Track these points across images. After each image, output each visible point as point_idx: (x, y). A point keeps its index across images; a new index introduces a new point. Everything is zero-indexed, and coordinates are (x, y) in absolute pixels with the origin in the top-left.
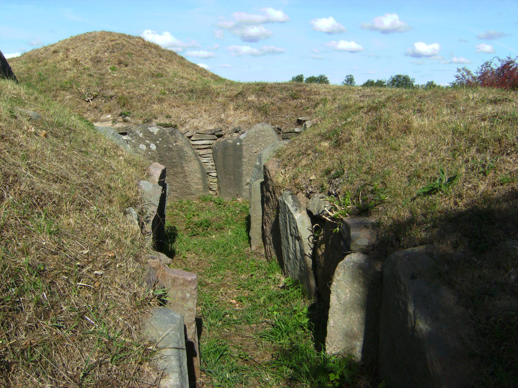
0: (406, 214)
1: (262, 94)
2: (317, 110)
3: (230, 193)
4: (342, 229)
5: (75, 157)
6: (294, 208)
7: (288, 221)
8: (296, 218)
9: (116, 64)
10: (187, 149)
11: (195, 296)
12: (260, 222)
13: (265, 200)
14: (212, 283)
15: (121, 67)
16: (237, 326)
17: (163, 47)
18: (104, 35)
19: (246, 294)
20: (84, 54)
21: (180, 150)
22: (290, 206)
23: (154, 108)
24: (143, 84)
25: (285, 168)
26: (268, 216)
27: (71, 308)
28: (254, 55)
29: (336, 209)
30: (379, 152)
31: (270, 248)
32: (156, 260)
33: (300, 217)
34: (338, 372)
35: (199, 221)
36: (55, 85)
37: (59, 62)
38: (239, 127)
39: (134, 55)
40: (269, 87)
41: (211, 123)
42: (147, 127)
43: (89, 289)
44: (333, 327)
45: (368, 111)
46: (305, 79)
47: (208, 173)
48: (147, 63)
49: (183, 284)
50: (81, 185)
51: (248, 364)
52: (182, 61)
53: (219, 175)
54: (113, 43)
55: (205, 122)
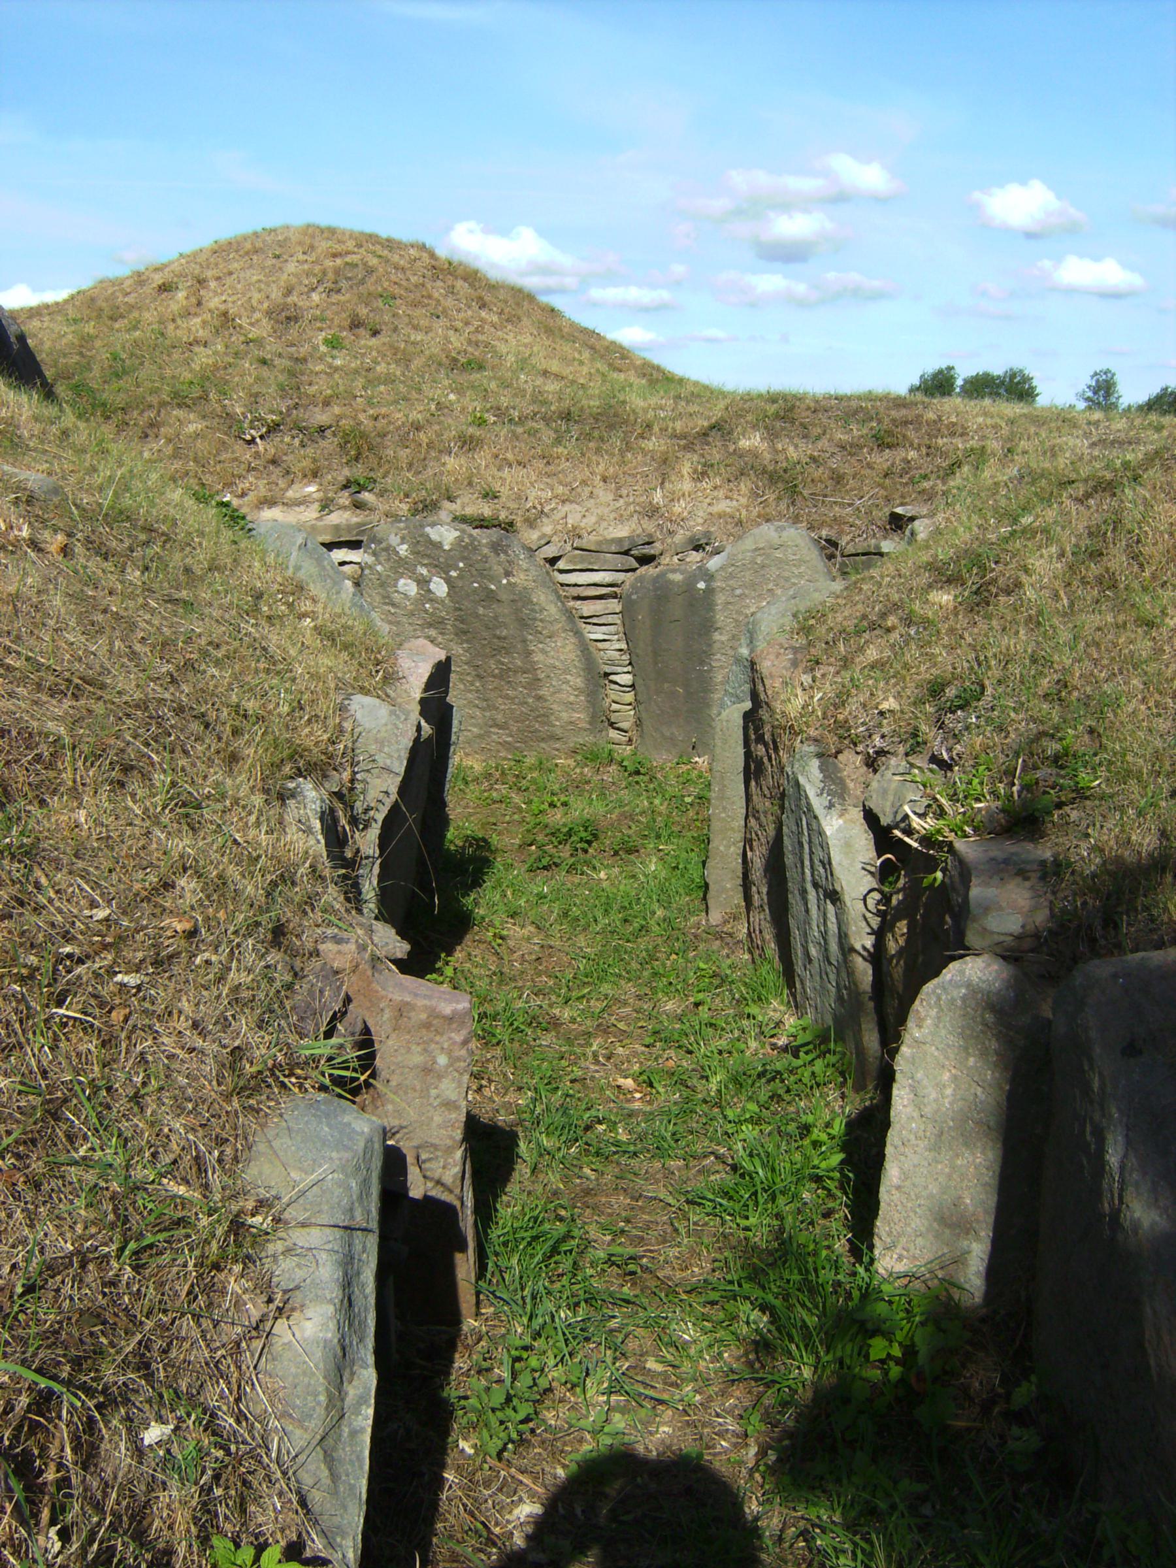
0: (1145, 840)
1: (783, 429)
2: (955, 482)
3: (672, 740)
4: (951, 877)
5: (148, 617)
6: (825, 799)
7: (805, 839)
8: (829, 830)
9: (342, 328)
10: (542, 597)
11: (462, 1064)
12: (739, 836)
13: (753, 770)
14: (573, 1020)
15: (357, 336)
16: (623, 1160)
17: (494, 275)
18: (313, 237)
19: (671, 1063)
20: (248, 294)
21: (521, 599)
22: (811, 792)
23: (449, 467)
24: (420, 391)
25: (812, 670)
26: (757, 819)
27: (22, 1083)
28: (801, 304)
29: (941, 813)
30: (1099, 629)
31: (762, 918)
32: (345, 948)
33: (839, 830)
34: (900, 1336)
35: (565, 825)
36: (154, 391)
37: (173, 320)
38: (707, 534)
39: (399, 301)
40: (808, 408)
41: (620, 519)
42: (422, 526)
43: (87, 1028)
44: (898, 1188)
45: (1088, 496)
46: (959, 382)
47: (607, 675)
48: (439, 326)
49: (427, 1026)
50: (143, 705)
51: (634, 1284)
52: (550, 322)
53: (639, 682)
54: (339, 261)
55: (604, 517)
